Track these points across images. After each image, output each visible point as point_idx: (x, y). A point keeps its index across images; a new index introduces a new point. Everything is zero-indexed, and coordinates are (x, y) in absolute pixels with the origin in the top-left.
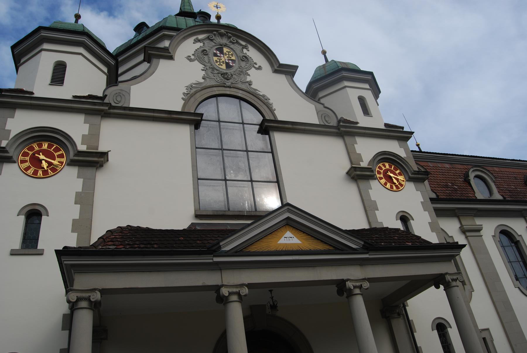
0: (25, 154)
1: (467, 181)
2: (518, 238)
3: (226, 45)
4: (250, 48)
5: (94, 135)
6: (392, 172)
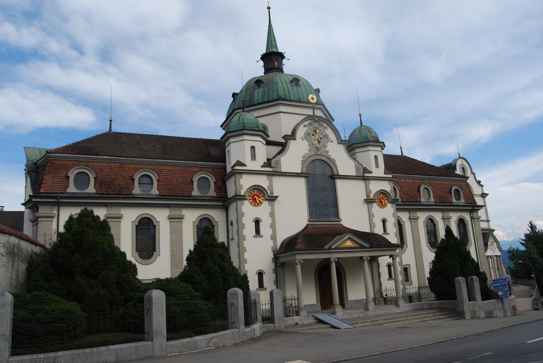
1: (419, 191)
2: (436, 223)
3: (318, 128)
5: (271, 186)
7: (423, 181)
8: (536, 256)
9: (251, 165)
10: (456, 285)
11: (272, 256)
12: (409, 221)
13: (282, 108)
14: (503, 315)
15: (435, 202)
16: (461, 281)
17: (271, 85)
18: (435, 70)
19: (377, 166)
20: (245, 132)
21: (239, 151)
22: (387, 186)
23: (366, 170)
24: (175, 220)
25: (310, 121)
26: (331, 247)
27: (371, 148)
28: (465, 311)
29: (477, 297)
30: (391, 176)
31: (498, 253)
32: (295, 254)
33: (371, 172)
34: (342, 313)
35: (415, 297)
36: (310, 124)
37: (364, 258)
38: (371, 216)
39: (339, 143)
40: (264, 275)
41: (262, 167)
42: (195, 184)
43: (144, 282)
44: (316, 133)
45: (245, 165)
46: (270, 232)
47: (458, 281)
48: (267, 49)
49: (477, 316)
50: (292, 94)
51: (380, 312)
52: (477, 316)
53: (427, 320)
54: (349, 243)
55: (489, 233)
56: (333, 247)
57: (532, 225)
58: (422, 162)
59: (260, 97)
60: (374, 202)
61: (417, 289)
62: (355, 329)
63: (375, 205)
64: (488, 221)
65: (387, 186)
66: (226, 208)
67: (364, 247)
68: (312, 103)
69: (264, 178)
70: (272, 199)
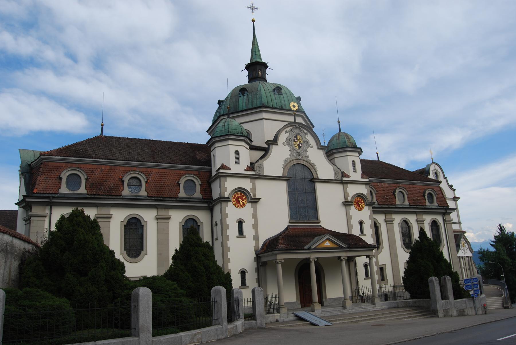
1: (395, 195)
3: (298, 134)
4: (309, 134)
5: (254, 189)
6: (242, 199)
7: (398, 185)
8: (506, 257)
9: (235, 169)
12: (385, 223)
13: (265, 115)
14: (474, 313)
15: (410, 205)
16: (434, 281)
17: (255, 94)
18: (409, 81)
20: (230, 137)
22: (364, 190)
23: (344, 175)
25: (291, 127)
26: (310, 247)
29: (449, 296)
30: (367, 180)
33: (349, 177)
34: (320, 311)
36: (291, 130)
37: (342, 258)
38: (349, 218)
39: (319, 149)
40: (246, 274)
41: (245, 170)
42: (182, 186)
45: (229, 169)
46: (253, 232)
47: (432, 281)
48: (251, 59)
49: (450, 314)
50: (275, 102)
51: (357, 310)
52: (450, 314)
53: (402, 318)
54: (327, 244)
55: (461, 235)
56: (312, 248)
57: (501, 227)
60: (352, 205)
61: (392, 288)
63: (352, 208)
64: (460, 223)
65: (364, 190)
66: (211, 210)
67: (341, 247)
68: (293, 111)
69: (248, 181)
70: (255, 201)
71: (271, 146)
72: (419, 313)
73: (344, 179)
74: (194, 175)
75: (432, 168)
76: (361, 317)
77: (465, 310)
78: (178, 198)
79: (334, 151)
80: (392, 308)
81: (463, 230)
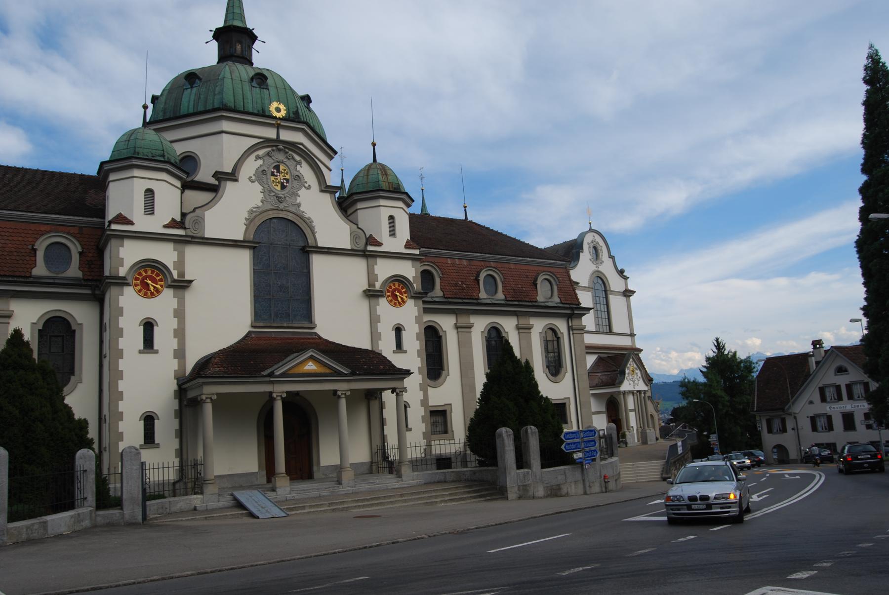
0: (137, 279)
1: (536, 285)
3: (283, 162)
4: (304, 164)
5: (180, 263)
6: (401, 293)
7: (487, 264)
8: (720, 393)
9: (142, 223)
10: (498, 441)
11: (174, 386)
12: (455, 331)
13: (226, 126)
14: (580, 490)
15: (506, 299)
16: (505, 435)
17: (226, 88)
18: (603, 97)
19: (393, 233)
20: (135, 162)
21: (125, 196)
22: (409, 270)
23: (372, 240)
24: (463, 329)
25: (269, 149)
26: (273, 372)
27: (382, 202)
28: (509, 484)
29: (532, 461)
30: (417, 252)
31: (642, 386)
32: (201, 385)
33: (379, 244)
34: (288, 489)
35: (459, 460)
36: (268, 154)
37: (339, 393)
38: (374, 320)
39: (322, 191)
40: (156, 421)
41: (165, 226)
42: (40, 255)
43: (553, 402)
44: (278, 171)
45: (132, 223)
46: (174, 344)
47: (501, 435)
48: (226, 21)
49: (531, 493)
50: (250, 101)
51: (364, 487)
52: (531, 493)
53: (436, 502)
54: (311, 366)
55: (629, 355)
56: (277, 373)
57: (718, 343)
58: (496, 232)
59: (192, 103)
60: (382, 296)
61: (462, 445)
62: (288, 519)
63: (383, 302)
64: (632, 335)
65: (409, 270)
66: (99, 300)
67: (340, 374)
68: (275, 118)
69: (170, 246)
70: (182, 285)
71: (223, 183)
72: (475, 492)
73: (370, 248)
74: (68, 233)
75: (588, 239)
76: (358, 501)
77: (562, 486)
78: (30, 277)
79: (356, 197)
80: (434, 483)
81: (638, 346)
